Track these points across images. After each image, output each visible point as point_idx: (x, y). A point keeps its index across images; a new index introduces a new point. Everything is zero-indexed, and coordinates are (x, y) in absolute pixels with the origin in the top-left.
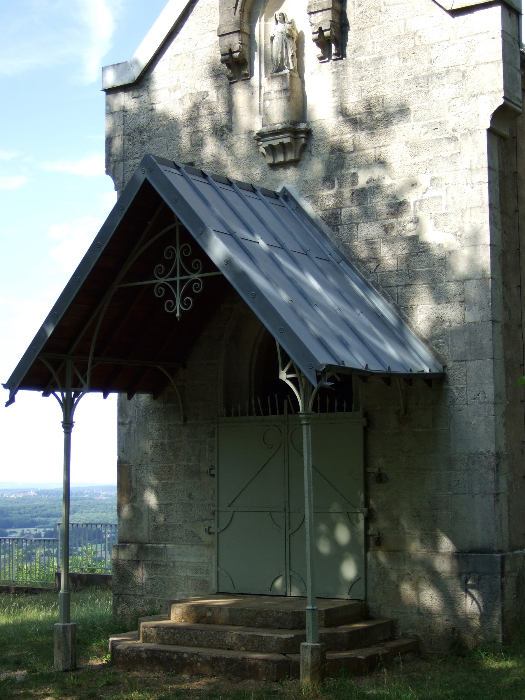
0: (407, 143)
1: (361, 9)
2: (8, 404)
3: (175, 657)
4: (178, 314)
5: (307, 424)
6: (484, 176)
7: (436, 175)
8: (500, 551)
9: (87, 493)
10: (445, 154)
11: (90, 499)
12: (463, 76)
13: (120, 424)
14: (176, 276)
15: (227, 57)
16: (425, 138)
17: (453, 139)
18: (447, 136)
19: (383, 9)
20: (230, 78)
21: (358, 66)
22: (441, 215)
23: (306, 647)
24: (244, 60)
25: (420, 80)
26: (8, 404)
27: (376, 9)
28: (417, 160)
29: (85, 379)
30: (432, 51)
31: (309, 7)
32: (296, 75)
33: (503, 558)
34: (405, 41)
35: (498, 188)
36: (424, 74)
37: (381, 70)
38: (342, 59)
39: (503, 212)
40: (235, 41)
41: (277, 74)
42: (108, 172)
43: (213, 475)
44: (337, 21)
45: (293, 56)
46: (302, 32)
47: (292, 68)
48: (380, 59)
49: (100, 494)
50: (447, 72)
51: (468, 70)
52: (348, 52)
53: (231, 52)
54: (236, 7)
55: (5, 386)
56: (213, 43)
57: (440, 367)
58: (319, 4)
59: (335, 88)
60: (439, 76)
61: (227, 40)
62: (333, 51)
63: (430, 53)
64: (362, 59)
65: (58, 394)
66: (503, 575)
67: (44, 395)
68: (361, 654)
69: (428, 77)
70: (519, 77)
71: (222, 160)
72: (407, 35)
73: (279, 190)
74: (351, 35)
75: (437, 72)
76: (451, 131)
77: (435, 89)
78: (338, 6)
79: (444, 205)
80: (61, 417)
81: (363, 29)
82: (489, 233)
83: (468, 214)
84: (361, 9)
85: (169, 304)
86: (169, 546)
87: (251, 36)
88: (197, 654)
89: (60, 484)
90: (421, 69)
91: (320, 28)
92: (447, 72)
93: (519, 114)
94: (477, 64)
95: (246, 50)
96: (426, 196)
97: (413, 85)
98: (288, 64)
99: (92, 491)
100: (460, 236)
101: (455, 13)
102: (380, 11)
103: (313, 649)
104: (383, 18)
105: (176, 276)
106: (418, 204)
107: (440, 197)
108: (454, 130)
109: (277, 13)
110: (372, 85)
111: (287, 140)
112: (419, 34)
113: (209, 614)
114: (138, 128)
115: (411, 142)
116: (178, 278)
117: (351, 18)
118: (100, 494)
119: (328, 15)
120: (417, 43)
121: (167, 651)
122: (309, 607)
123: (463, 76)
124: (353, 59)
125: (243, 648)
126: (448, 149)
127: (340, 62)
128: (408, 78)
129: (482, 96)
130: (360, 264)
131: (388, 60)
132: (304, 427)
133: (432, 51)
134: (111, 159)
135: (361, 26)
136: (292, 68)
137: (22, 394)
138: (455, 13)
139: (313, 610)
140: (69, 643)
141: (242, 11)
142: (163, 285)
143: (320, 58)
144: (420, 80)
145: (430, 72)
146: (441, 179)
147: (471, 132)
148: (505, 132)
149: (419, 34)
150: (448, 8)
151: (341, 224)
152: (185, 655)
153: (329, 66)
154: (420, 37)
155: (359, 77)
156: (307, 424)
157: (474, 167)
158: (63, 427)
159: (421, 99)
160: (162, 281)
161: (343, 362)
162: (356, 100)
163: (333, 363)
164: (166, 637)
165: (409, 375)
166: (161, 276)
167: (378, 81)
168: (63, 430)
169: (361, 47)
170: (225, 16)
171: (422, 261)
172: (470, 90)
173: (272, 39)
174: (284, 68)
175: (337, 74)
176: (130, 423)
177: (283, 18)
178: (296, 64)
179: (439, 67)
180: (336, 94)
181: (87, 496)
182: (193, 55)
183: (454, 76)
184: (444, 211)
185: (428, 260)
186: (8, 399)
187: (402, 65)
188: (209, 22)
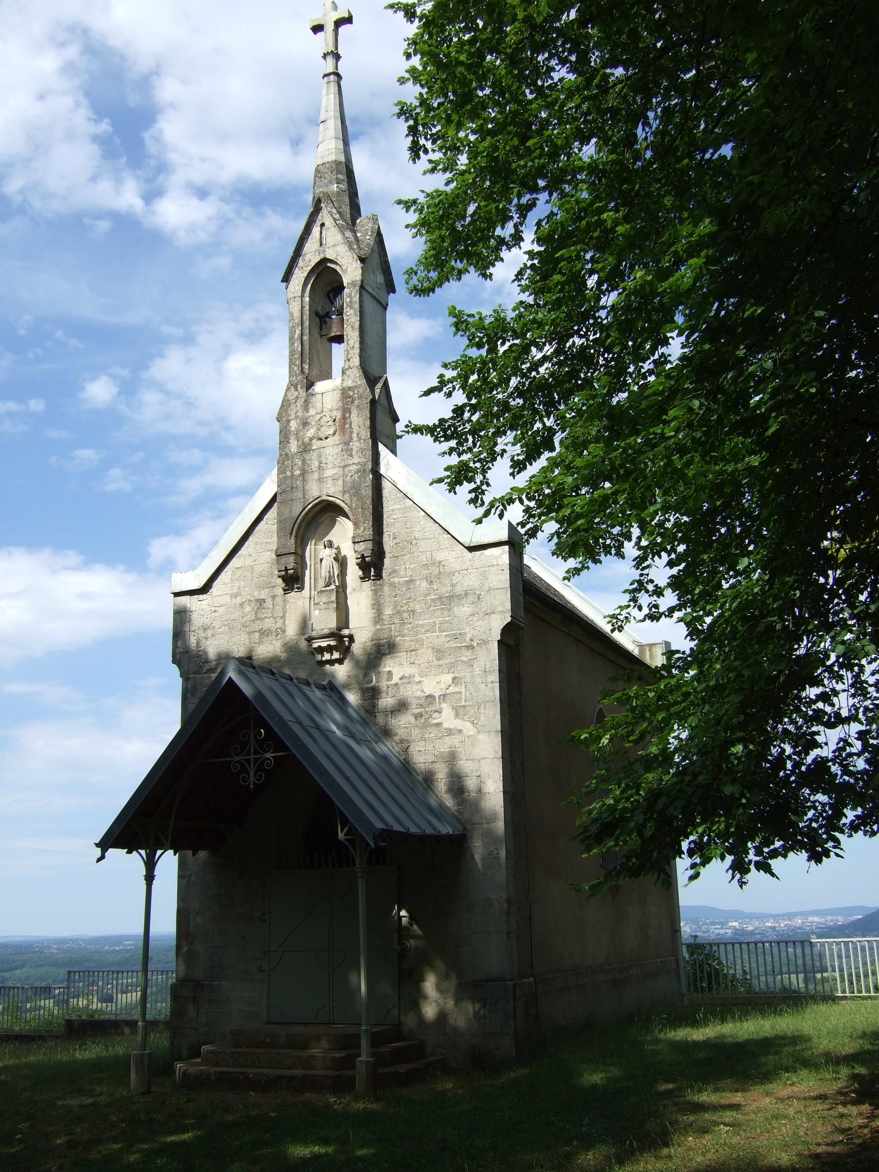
0: (433, 648)
1: (395, 541)
2: (99, 860)
3: (242, 1077)
4: (251, 786)
5: (362, 877)
6: (495, 677)
7: (457, 675)
8: (512, 980)
9: (37, 947)
10: (464, 659)
11: (41, 953)
12: (479, 598)
13: (180, 877)
14: (250, 755)
15: (283, 573)
16: (448, 645)
17: (470, 647)
18: (466, 644)
19: (413, 542)
20: (284, 590)
21: (393, 585)
22: (460, 706)
23: (361, 1062)
24: (298, 576)
25: (444, 600)
26: (99, 860)
27: (408, 542)
28: (441, 662)
29: (167, 841)
30: (454, 578)
31: (354, 537)
32: (341, 590)
33: (514, 985)
34: (432, 568)
35: (506, 686)
36: (447, 595)
37: (412, 590)
38: (379, 579)
39: (509, 705)
40: (290, 562)
41: (325, 589)
42: (174, 662)
43: (265, 920)
44: (376, 549)
45: (338, 575)
46: (345, 556)
47: (337, 584)
48: (411, 581)
49: (51, 947)
50: (466, 594)
51: (483, 593)
52: (384, 575)
53: (286, 570)
54: (291, 534)
55: (97, 845)
56: (270, 560)
57: (461, 828)
58: (362, 536)
59: (373, 602)
60: (459, 597)
61: (284, 560)
62: (372, 573)
63: (452, 579)
64: (396, 580)
65: (143, 852)
66: (515, 999)
67: (127, 853)
68: (402, 1069)
69: (451, 598)
70: (522, 599)
71: (402, 706)
72: (433, 564)
73: (325, 683)
74: (387, 562)
75: (458, 594)
76: (469, 641)
77: (455, 608)
78: (377, 537)
79: (464, 699)
80: (143, 870)
81: (397, 557)
82: (496, 722)
83: (482, 707)
84: (395, 541)
85: (244, 778)
86: (223, 983)
87: (303, 557)
88: (261, 1074)
89: (141, 931)
90: (445, 590)
91: (363, 555)
92: (466, 594)
93: (522, 628)
94: (490, 589)
95: (299, 567)
96: (448, 691)
97: (438, 603)
98: (334, 582)
99: (43, 944)
100: (477, 724)
101: (472, 549)
102: (411, 544)
103: (367, 1063)
104: (414, 549)
105: (250, 755)
106: (442, 697)
107: (460, 693)
108: (471, 640)
109: (326, 539)
110: (405, 602)
111: (333, 643)
112: (443, 563)
113: (268, 1040)
114: (202, 626)
115: (436, 648)
116: (252, 757)
117: (387, 548)
118: (51, 947)
119: (369, 545)
120: (442, 571)
121: (234, 1073)
122: (364, 1028)
123: (479, 598)
124: (389, 580)
125: (300, 1067)
126: (466, 656)
127: (378, 582)
128: (433, 597)
129: (494, 615)
130: (394, 744)
131: (418, 582)
132: (360, 879)
133: (454, 578)
134: (178, 651)
135: (395, 555)
136: (337, 584)
137: (112, 852)
138: (472, 549)
139: (367, 1030)
140: (146, 1068)
141: (296, 536)
142: (238, 762)
143: (361, 578)
144: (444, 600)
145: (452, 594)
146: (461, 679)
147: (485, 642)
148: (511, 642)
149: (443, 563)
150: (467, 545)
151: (378, 712)
152: (251, 1075)
153: (367, 585)
154: (444, 566)
155: (394, 594)
156: (362, 877)
157: (487, 670)
158: (145, 879)
159: (444, 615)
160: (238, 758)
161: (392, 827)
162: (391, 612)
163: (386, 828)
164: (231, 1061)
165: (439, 836)
166: (238, 755)
167: (410, 599)
168: (145, 882)
169: (395, 571)
170: (282, 540)
171: (445, 743)
172: (484, 609)
173: (321, 560)
174: (331, 584)
175: (375, 592)
176: (190, 876)
177: (330, 545)
178: (340, 581)
179: (459, 590)
180: (375, 607)
181: (37, 949)
182: (253, 569)
183: (471, 598)
184: (463, 704)
185: (450, 743)
186: (99, 855)
187: (429, 587)
188: (266, 543)
